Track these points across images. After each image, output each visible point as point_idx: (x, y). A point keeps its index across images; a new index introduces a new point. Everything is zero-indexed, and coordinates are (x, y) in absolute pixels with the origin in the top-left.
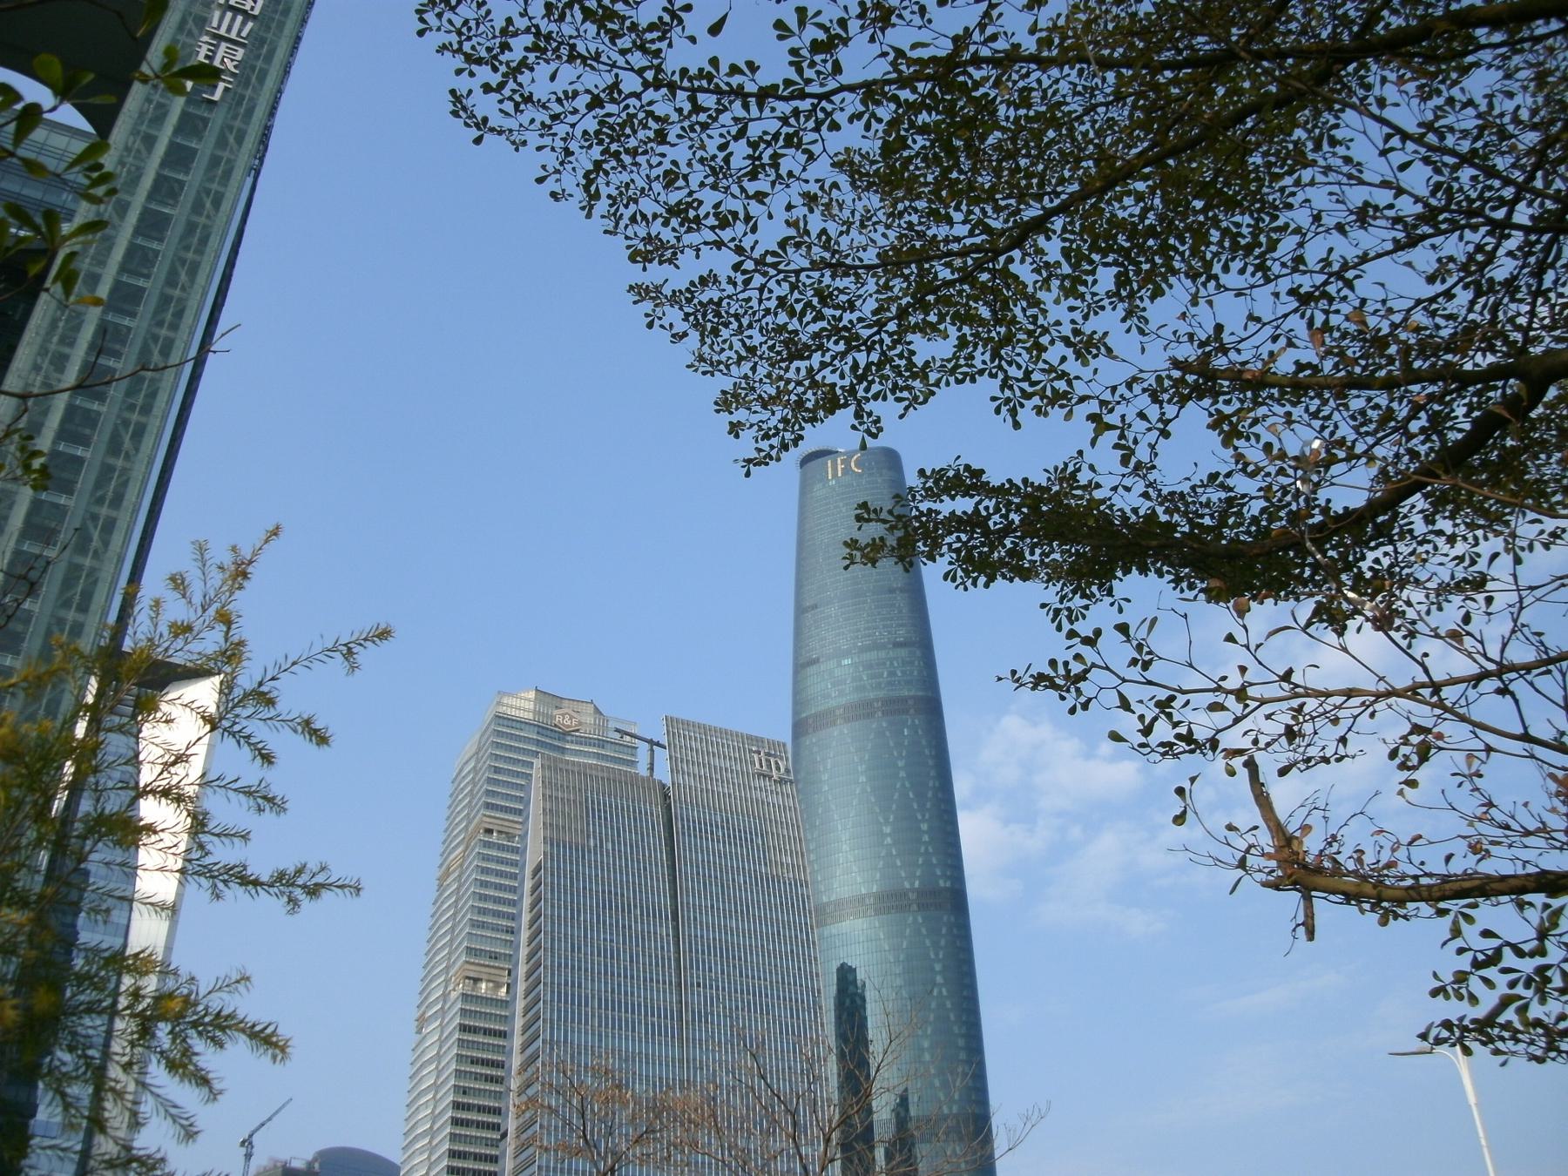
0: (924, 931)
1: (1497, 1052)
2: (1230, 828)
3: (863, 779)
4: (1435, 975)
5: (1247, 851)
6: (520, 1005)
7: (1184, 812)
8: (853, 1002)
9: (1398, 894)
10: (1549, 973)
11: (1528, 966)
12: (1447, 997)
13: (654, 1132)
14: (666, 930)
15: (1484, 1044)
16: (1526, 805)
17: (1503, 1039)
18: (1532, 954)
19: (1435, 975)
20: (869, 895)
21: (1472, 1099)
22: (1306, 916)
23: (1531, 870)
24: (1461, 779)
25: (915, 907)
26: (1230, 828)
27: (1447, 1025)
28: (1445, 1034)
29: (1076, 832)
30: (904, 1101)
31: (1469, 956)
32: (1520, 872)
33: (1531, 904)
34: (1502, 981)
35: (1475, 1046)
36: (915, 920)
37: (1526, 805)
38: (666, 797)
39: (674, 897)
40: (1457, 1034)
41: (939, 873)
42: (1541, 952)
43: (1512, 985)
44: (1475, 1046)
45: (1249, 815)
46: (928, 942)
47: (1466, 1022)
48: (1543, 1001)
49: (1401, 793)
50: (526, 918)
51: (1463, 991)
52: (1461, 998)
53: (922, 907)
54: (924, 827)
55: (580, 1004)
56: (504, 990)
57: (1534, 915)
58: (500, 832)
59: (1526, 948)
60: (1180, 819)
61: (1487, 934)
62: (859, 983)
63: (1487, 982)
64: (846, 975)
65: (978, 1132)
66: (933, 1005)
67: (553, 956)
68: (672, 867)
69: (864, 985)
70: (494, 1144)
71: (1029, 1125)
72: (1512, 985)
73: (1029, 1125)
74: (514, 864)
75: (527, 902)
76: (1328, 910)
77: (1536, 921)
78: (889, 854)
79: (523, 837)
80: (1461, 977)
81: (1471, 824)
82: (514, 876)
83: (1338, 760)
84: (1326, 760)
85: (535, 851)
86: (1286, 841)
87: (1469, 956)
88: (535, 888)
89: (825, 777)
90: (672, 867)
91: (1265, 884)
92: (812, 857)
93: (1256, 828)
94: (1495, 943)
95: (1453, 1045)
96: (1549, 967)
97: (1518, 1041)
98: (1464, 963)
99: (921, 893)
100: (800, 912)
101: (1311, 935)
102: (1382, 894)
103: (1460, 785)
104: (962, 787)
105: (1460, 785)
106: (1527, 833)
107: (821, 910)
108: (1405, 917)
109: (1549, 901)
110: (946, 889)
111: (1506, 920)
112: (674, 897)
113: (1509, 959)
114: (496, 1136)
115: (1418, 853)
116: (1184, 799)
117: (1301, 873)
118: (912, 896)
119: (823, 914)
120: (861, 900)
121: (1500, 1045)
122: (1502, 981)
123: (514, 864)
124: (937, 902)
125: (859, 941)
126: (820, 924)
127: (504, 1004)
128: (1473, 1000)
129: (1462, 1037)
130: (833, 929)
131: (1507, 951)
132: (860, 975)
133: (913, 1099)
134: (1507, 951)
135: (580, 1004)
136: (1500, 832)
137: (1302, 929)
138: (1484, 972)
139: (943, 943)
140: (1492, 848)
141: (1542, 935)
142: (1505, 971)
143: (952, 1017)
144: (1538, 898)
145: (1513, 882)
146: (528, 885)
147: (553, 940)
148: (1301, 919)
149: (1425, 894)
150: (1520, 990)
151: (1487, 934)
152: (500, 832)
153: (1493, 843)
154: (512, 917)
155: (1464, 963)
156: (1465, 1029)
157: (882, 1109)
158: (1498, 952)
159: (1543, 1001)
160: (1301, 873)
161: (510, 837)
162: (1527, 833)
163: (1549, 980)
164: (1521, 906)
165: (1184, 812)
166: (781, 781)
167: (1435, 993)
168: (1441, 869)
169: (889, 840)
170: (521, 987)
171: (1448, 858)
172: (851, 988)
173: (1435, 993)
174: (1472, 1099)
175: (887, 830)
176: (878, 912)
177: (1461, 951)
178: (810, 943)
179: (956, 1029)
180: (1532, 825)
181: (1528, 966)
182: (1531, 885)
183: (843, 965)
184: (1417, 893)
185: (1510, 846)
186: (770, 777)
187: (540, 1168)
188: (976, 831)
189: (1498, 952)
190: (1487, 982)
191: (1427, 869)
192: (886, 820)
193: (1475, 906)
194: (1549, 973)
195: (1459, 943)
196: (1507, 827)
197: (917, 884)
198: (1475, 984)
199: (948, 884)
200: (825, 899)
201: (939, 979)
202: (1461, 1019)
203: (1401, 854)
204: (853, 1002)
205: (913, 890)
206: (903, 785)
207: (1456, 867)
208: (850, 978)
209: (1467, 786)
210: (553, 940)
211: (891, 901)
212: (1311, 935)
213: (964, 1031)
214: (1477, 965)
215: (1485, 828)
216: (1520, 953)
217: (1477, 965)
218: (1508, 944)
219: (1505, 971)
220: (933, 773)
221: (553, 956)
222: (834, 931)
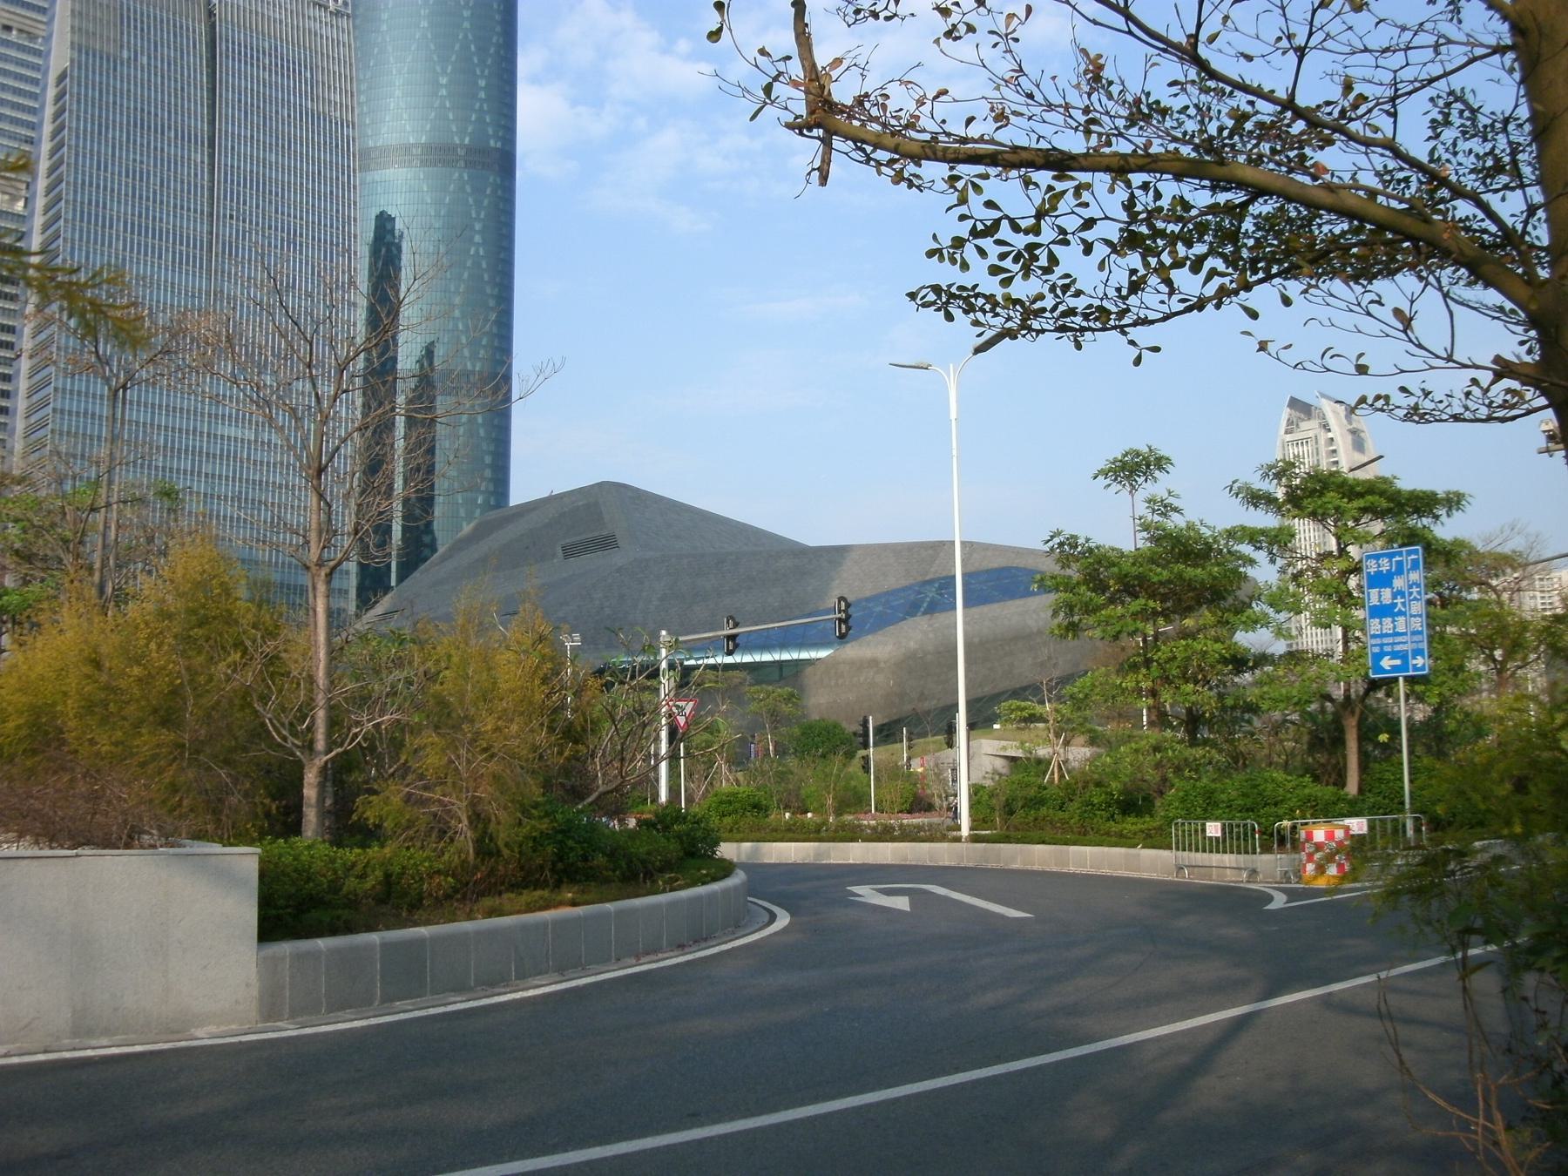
0: (468, 189)
1: (976, 323)
2: (763, 52)
3: (424, 24)
4: (935, 237)
5: (776, 79)
6: (38, 221)
7: (720, 30)
8: (389, 250)
9: (915, 148)
10: (1037, 252)
11: (1020, 241)
12: (941, 259)
13: (168, 352)
14: (200, 156)
15: (966, 312)
16: (1054, 78)
17: (984, 312)
18: (1027, 232)
19: (935, 237)
20: (415, 145)
21: (953, 415)
22: (823, 161)
23: (1043, 145)
24: (996, 39)
25: (462, 163)
26: (763, 52)
27: (937, 289)
28: (932, 297)
29: (641, 123)
30: (429, 352)
31: (970, 223)
32: (1034, 145)
33: (1036, 185)
34: (994, 251)
35: (957, 313)
36: (461, 177)
37: (1054, 78)
38: (211, 14)
39: (212, 122)
40: (945, 300)
41: (490, 131)
42: (1036, 230)
43: (1003, 256)
44: (957, 313)
45: (785, 41)
46: (471, 200)
47: (953, 290)
48: (1026, 276)
49: (937, 41)
50: (48, 128)
51: (957, 256)
52: (953, 261)
53: (469, 164)
54: (482, 83)
55: (104, 226)
56: (21, 204)
57: (1037, 196)
58: (20, 31)
59: (1024, 224)
60: (715, 35)
61: (990, 204)
62: (397, 233)
63: (982, 252)
64: (384, 223)
65: (496, 390)
66: (469, 264)
67: (76, 173)
68: (212, 90)
69: (401, 236)
70: (8, 362)
71: (541, 378)
72: (1003, 256)
73: (541, 378)
74: (36, 68)
75: (49, 110)
76: (845, 163)
77: (1038, 202)
78: (442, 106)
79: (47, 39)
80: (958, 243)
81: (998, 88)
82: (35, 82)
83: (887, 18)
84: (875, 15)
85: (60, 57)
86: (816, 83)
87: (970, 223)
88: (60, 97)
89: (385, 16)
90: (212, 90)
91: (789, 126)
92: (363, 98)
93: (789, 58)
94: (996, 214)
95: (939, 310)
96: (1039, 246)
97: (997, 315)
98: (964, 230)
99: (470, 150)
100: (345, 155)
101: (824, 180)
102: (903, 149)
103: (995, 45)
104: (527, 62)
105: (995, 45)
106: (1050, 107)
107: (365, 154)
108: (918, 187)
109: (1054, 183)
110: (496, 149)
111: (1012, 195)
112: (212, 122)
113: (1005, 231)
114: (9, 354)
115: (941, 109)
116: (722, 15)
117: (824, 117)
118: (461, 152)
119: (368, 159)
120: (407, 149)
121: (979, 315)
122: (994, 251)
123: (36, 68)
124: (486, 161)
125: (400, 190)
126: (365, 168)
127: (20, 218)
128: (965, 266)
129: (948, 302)
130: (377, 175)
131: (1005, 223)
132: (399, 225)
133: (439, 352)
134: (1005, 223)
135: (104, 226)
136: (1023, 100)
137: (816, 173)
138: (979, 242)
139: (486, 202)
140: (1013, 118)
141: (1040, 215)
142: (999, 242)
143: (486, 277)
144: (1044, 177)
145: (1024, 155)
146: (51, 92)
147: (77, 155)
148: (817, 164)
149: (940, 154)
150: (1007, 263)
151: (990, 204)
152: (20, 31)
153: (1014, 113)
154: (31, 126)
155: (964, 230)
156: (952, 296)
157: (407, 357)
158: (997, 222)
159: (1026, 276)
160: (824, 117)
161: (32, 37)
162: (1050, 107)
163: (1037, 259)
164: (1027, 183)
165: (720, 30)
166: (337, 14)
167: (931, 254)
168: (960, 131)
169: (444, 92)
170: (40, 202)
171: (970, 121)
172: (389, 237)
173: (931, 254)
174: (953, 415)
175: (443, 80)
176: (424, 163)
177: (963, 218)
178: (351, 187)
179: (488, 290)
180: (1056, 100)
181: (1020, 241)
182: (1040, 161)
183: (382, 213)
184: (930, 151)
185: (1030, 118)
186: (326, 8)
187: (56, 389)
188: (538, 110)
189: (997, 222)
190: (982, 252)
191: (947, 128)
192: (444, 72)
193: (986, 177)
194: (1037, 252)
195: (963, 210)
196: (1030, 96)
197: (467, 141)
198: (969, 252)
199: (499, 145)
200: (371, 144)
201: (477, 239)
202: (950, 286)
203: (926, 109)
204: (389, 250)
205: (462, 146)
206: (466, 37)
207: (974, 131)
208: (389, 227)
209: (1002, 46)
210: (77, 155)
211: (438, 154)
212: (824, 180)
213: (496, 291)
214: (975, 233)
215: (1009, 93)
216: (1016, 228)
217: (975, 233)
218: (1007, 217)
219: (999, 242)
220: (498, 29)
221: (76, 173)
222: (377, 178)
